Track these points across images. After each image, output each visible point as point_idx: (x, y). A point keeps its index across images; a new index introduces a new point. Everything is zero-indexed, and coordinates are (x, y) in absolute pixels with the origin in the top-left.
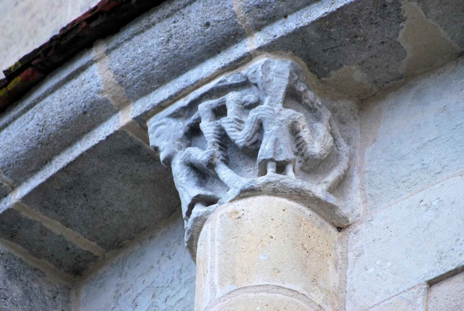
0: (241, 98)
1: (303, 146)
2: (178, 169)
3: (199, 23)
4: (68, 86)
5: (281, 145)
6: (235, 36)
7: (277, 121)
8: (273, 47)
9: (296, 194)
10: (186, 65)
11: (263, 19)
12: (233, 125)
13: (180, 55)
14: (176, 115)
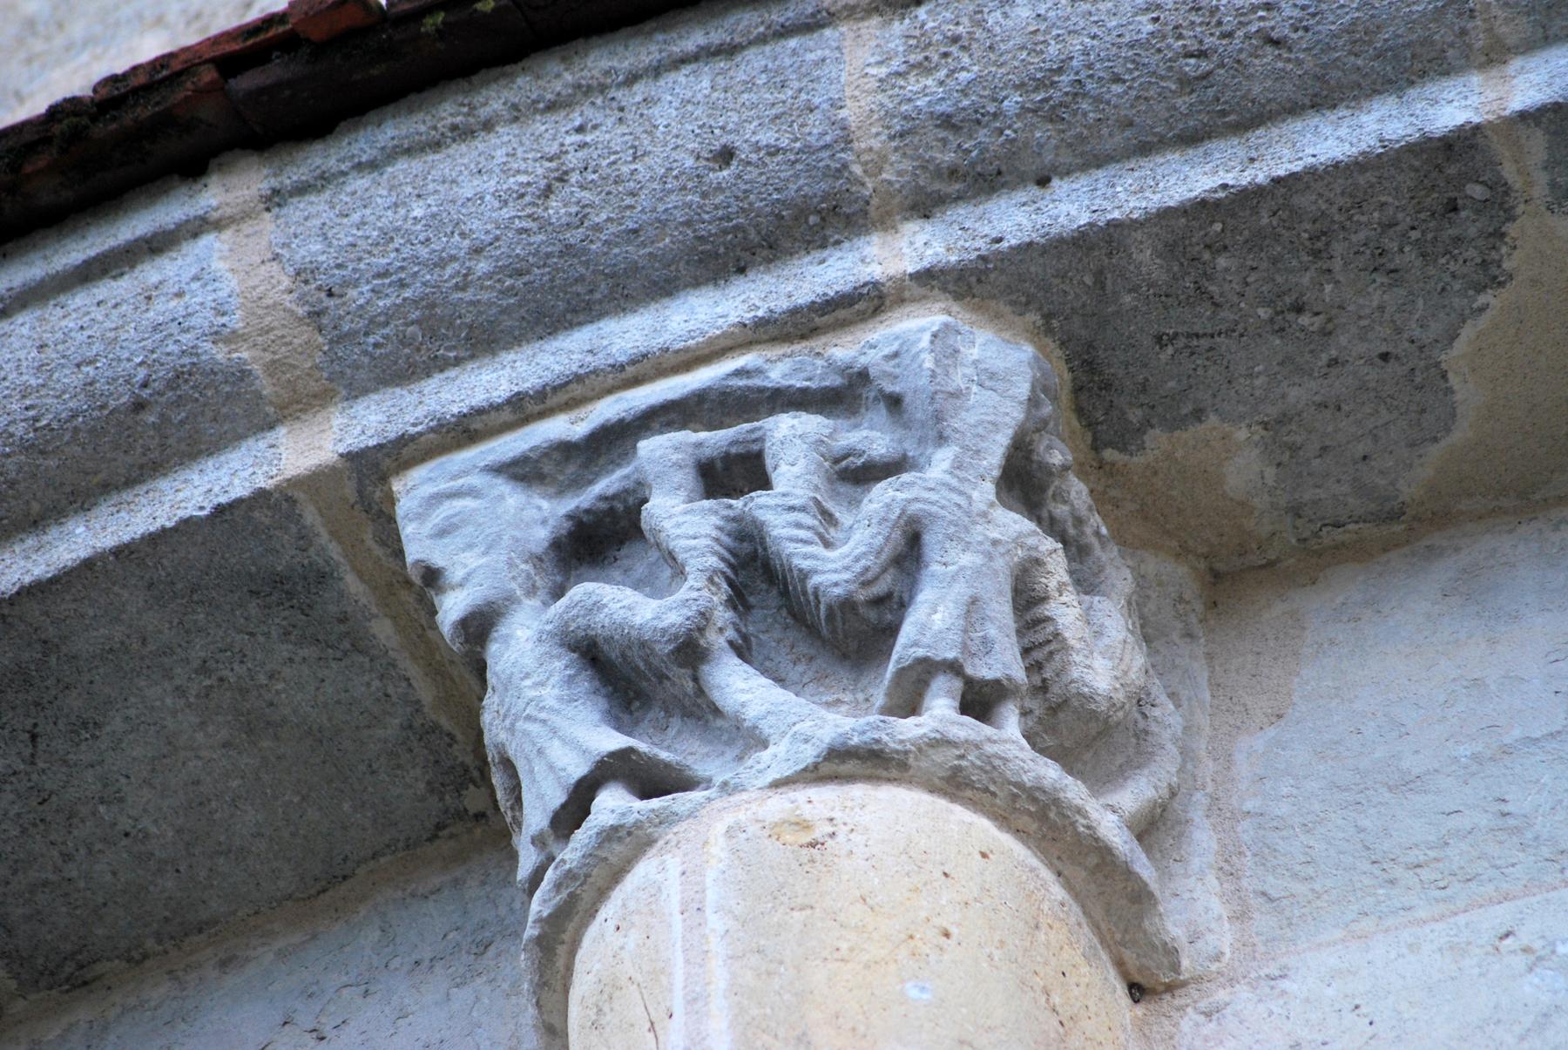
0: (830, 436)
1: (1051, 653)
2: (523, 652)
3: (690, 146)
4: (80, 299)
5: (988, 624)
6: (828, 217)
7: (980, 538)
8: (979, 281)
9: (1033, 809)
10: (598, 296)
11: (953, 173)
12: (807, 519)
13: (585, 251)
14: (523, 471)
